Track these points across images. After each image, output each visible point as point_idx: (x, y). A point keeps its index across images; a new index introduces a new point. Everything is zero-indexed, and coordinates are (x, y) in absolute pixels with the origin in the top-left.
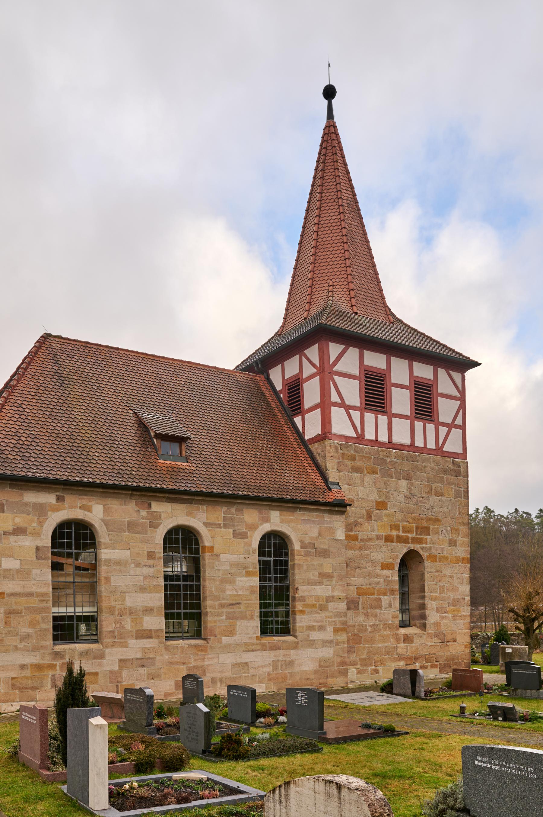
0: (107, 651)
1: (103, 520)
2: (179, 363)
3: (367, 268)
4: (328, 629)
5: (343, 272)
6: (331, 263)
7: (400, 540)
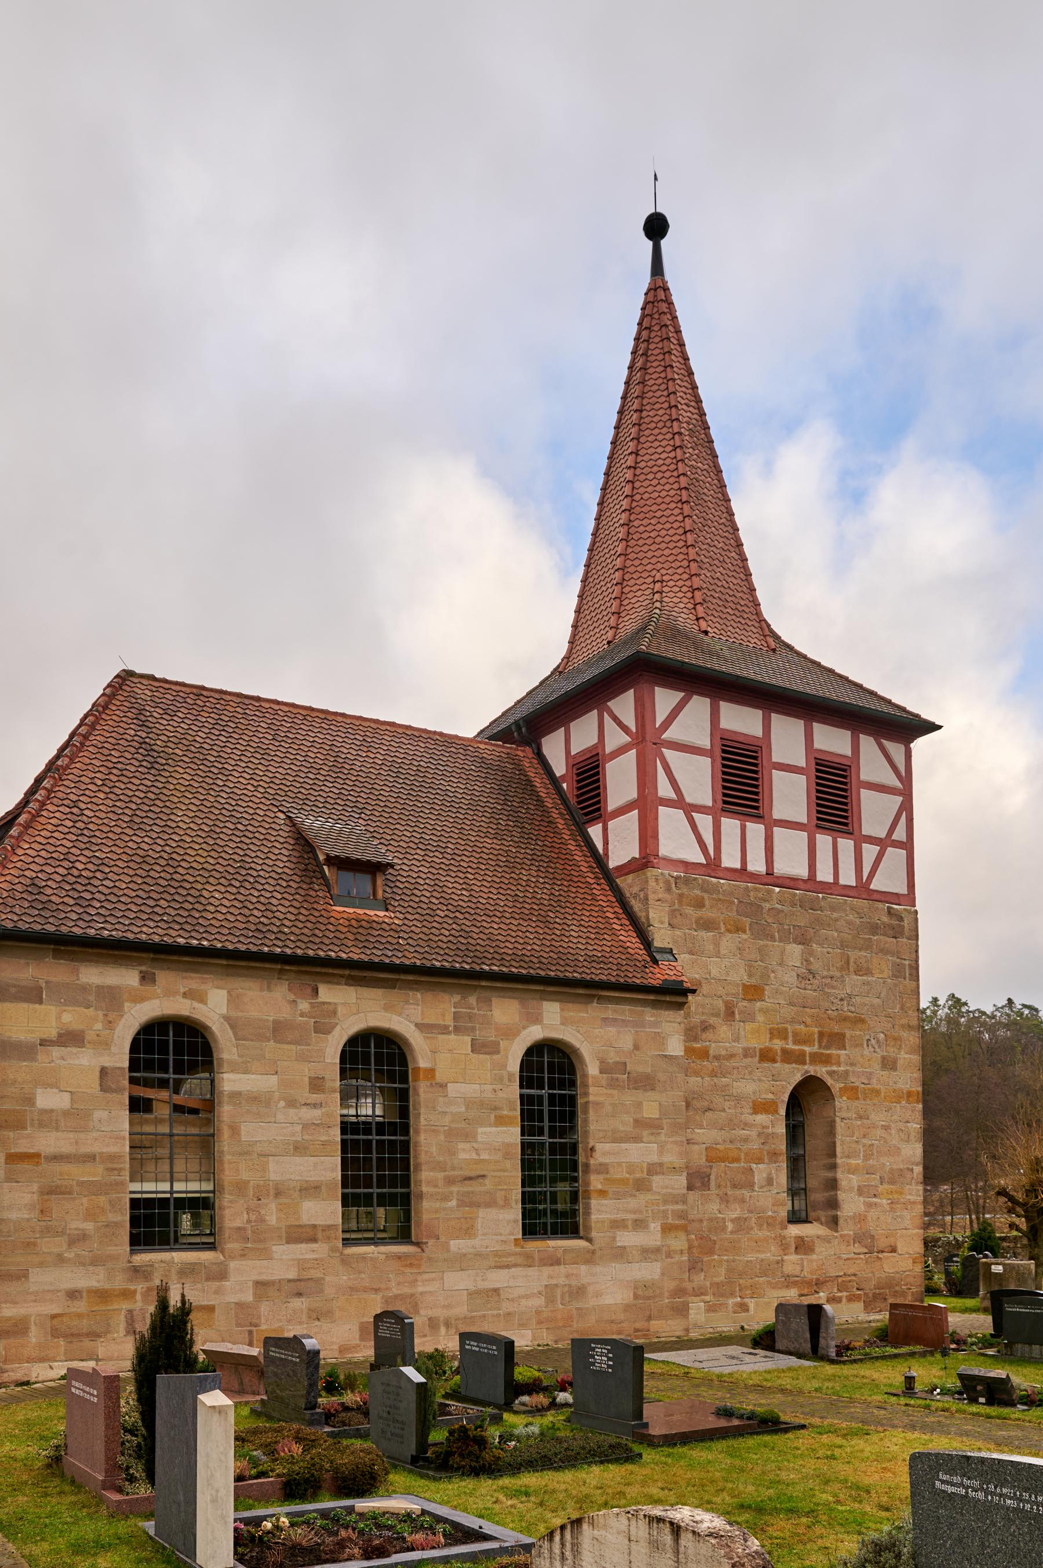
0: (232, 1265)
1: (227, 1018)
2: (372, 725)
3: (726, 548)
4: (652, 1225)
7: (789, 1057)
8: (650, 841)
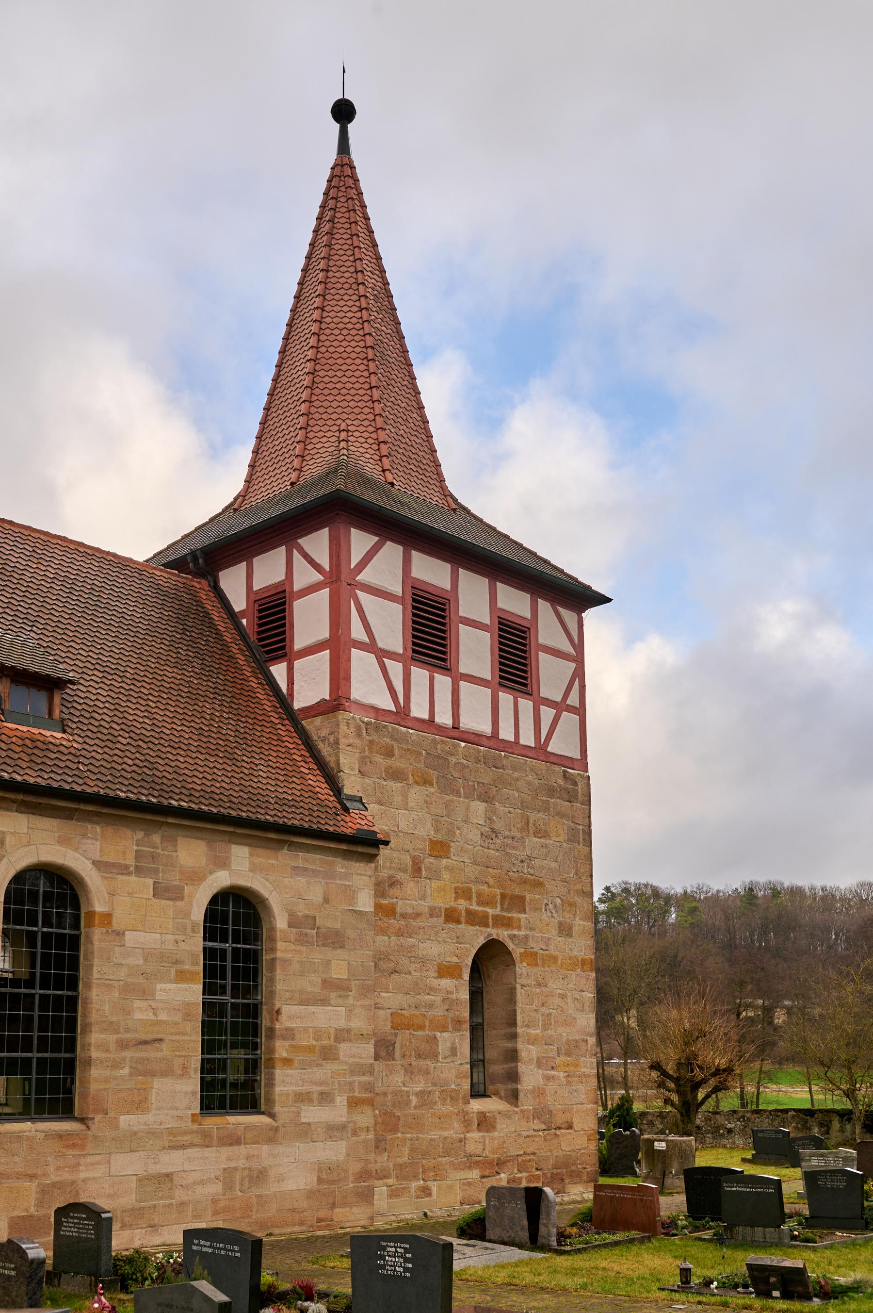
2: (42, 537)
3: (409, 408)
5: (367, 410)
6: (344, 391)
7: (474, 919)
8: (342, 682)
